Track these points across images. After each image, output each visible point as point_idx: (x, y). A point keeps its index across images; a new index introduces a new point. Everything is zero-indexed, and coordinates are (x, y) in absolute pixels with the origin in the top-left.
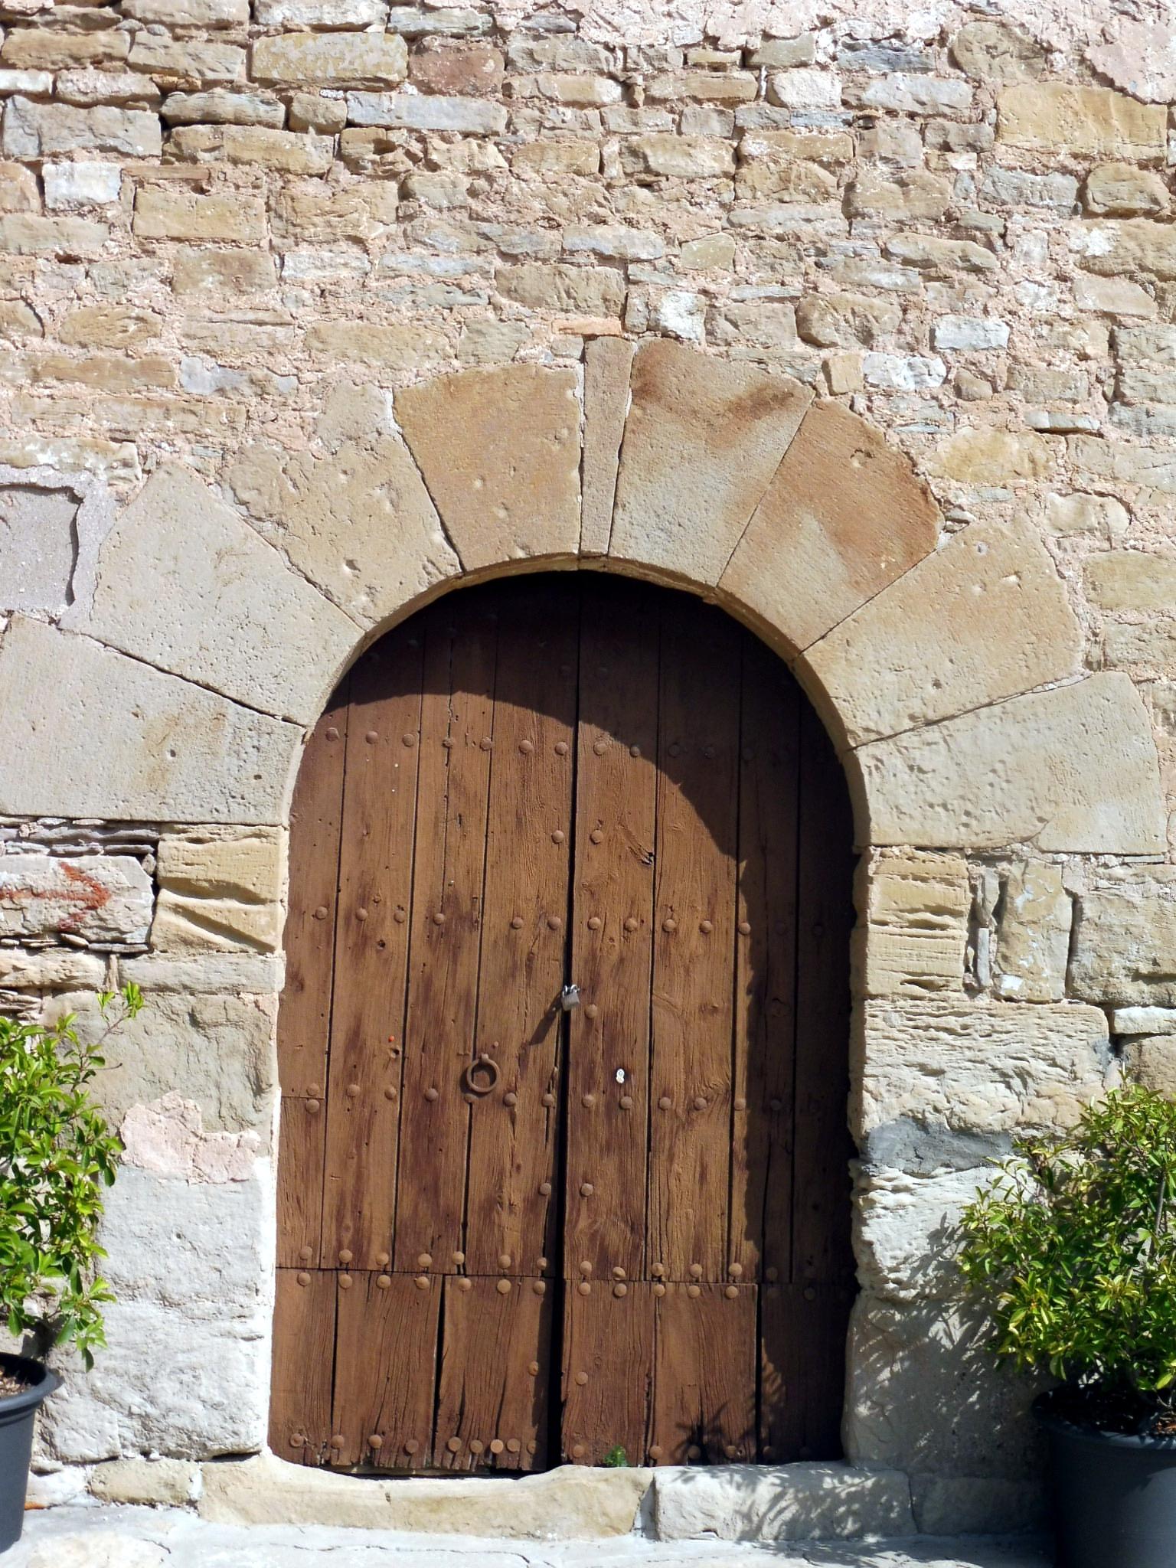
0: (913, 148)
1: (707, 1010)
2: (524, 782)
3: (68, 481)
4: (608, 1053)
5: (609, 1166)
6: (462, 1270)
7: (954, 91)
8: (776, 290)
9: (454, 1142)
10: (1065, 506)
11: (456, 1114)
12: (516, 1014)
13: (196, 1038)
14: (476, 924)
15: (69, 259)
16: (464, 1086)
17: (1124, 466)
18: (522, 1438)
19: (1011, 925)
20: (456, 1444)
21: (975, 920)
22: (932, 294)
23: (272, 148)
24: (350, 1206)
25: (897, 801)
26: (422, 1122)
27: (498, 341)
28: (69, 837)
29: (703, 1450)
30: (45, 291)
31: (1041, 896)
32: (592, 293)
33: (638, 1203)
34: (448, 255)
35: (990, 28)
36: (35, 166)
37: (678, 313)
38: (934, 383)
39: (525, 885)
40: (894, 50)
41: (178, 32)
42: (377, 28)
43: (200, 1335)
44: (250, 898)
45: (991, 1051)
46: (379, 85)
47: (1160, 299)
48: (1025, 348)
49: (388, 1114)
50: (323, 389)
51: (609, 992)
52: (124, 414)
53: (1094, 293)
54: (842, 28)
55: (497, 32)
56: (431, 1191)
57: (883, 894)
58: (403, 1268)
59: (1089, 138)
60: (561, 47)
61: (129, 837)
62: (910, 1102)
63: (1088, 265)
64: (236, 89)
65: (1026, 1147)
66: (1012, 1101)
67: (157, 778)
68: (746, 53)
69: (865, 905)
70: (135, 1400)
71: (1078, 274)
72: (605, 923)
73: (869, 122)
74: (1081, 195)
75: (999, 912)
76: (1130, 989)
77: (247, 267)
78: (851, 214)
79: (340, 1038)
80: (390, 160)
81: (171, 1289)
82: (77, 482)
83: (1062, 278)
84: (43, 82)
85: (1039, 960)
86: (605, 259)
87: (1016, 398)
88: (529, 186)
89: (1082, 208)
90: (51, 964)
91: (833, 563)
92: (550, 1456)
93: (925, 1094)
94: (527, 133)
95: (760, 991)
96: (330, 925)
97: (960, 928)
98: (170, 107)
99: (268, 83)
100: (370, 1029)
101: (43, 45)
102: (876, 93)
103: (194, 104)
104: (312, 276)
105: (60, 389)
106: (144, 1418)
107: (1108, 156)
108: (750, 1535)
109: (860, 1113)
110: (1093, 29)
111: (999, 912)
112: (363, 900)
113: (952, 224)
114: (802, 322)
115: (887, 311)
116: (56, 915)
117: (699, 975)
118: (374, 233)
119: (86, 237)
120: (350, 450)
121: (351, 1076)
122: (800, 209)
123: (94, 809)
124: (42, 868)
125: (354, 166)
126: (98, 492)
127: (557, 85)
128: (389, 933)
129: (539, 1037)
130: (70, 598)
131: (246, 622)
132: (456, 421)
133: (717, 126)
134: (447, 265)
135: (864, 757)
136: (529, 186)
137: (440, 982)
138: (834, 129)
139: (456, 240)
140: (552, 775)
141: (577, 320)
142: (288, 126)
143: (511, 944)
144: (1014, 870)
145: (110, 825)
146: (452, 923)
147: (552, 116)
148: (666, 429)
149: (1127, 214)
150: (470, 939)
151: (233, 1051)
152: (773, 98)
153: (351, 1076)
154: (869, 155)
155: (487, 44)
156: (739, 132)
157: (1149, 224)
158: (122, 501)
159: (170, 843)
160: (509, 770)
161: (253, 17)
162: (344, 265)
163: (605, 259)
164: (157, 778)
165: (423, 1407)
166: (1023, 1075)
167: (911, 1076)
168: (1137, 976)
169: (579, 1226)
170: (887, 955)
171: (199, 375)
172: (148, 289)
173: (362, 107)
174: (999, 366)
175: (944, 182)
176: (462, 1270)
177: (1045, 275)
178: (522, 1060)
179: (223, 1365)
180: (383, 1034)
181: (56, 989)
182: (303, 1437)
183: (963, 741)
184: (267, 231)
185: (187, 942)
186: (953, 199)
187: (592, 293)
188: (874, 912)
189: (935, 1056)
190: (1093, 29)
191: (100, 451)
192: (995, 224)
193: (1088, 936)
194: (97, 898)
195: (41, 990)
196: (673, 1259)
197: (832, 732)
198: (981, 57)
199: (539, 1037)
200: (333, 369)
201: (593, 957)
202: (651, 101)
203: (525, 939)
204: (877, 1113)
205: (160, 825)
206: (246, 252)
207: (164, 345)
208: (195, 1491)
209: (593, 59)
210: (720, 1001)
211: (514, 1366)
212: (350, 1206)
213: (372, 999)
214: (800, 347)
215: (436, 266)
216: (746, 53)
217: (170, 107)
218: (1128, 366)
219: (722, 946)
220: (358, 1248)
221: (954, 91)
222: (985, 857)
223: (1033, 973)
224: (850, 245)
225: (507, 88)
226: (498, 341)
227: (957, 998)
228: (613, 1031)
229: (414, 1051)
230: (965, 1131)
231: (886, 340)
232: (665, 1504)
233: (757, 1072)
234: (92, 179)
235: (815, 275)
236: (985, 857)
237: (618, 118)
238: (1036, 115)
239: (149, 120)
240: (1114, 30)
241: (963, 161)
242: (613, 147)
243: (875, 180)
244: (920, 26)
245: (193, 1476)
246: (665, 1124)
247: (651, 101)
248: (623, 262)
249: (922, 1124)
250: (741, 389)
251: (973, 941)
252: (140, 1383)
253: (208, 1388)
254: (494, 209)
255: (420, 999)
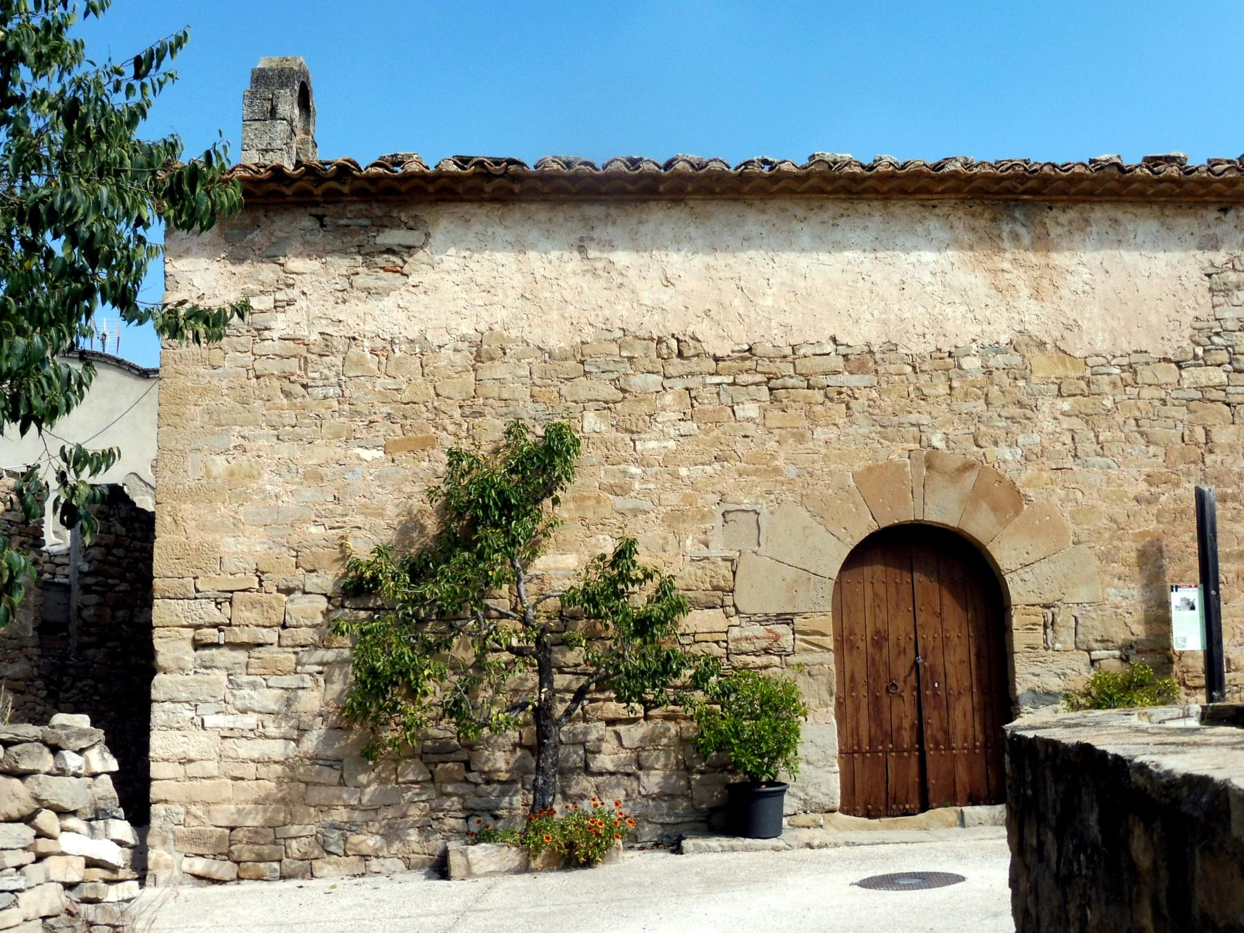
0: (1006, 381)
1: (962, 662)
2: (898, 593)
3: (755, 508)
4: (932, 678)
5: (936, 713)
6: (892, 750)
7: (1016, 360)
8: (967, 431)
9: (886, 710)
10: (1062, 493)
11: (886, 701)
12: (902, 668)
13: (811, 680)
14: (887, 639)
15: (745, 436)
16: (888, 691)
17: (1080, 479)
18: (914, 804)
19: (1057, 628)
20: (894, 807)
21: (1045, 627)
22: (1015, 428)
23: (806, 396)
24: (855, 732)
25: (1019, 591)
26: (876, 703)
27: (882, 454)
28: (767, 620)
29: (974, 801)
30: (740, 447)
31: (1064, 617)
32: (910, 436)
33: (945, 725)
34: (864, 428)
35: (1026, 338)
36: (732, 407)
37: (937, 441)
38: (1018, 457)
39: (899, 627)
40: (997, 349)
41: (771, 359)
42: (833, 354)
43: (820, 772)
44: (823, 635)
45: (1054, 667)
46: (836, 373)
47: (1087, 422)
48: (1046, 443)
49: (864, 702)
50: (830, 473)
51: (930, 657)
52: (769, 485)
53: (1066, 423)
54: (979, 342)
55: (871, 352)
56: (880, 725)
57: (1017, 620)
58: (873, 751)
59: (1060, 372)
60: (892, 356)
61: (785, 619)
62: (1030, 685)
63: (1063, 414)
64: (791, 377)
65: (1067, 697)
66: (1061, 682)
67: (792, 600)
68: (950, 353)
69: (1011, 624)
70: (801, 795)
71: (1060, 417)
72: (928, 637)
73: (991, 373)
74: (1059, 389)
75: (1052, 624)
76: (1095, 645)
77: (803, 436)
78: (987, 403)
79: (847, 678)
80: (845, 398)
81: (810, 759)
82: (757, 508)
83: (1055, 419)
84: (731, 379)
85: (1066, 638)
86: (913, 425)
87: (1044, 459)
88: (887, 402)
89: (1060, 394)
90: (764, 660)
91: (992, 517)
92: (924, 807)
93: (1034, 682)
94: (884, 385)
95: (978, 655)
96: (844, 643)
97: (1041, 629)
98: (772, 384)
99: (802, 375)
100: (857, 676)
101: (730, 368)
102: (992, 363)
103: (779, 382)
104: (822, 437)
105: (748, 479)
106: (805, 800)
107: (1066, 377)
108: (995, 824)
109: (1015, 689)
110: (1058, 335)
111: (1052, 624)
112: (851, 634)
113: (1020, 404)
114: (976, 441)
115: (1001, 434)
116: (765, 644)
117: (959, 650)
118: (840, 422)
119: (750, 429)
120: (841, 493)
121: (852, 690)
122: (973, 403)
123: (773, 610)
124: (759, 630)
125: (831, 400)
126: (764, 512)
127: (892, 369)
128: (862, 645)
129: (909, 675)
130: (759, 545)
131: (814, 548)
132: (874, 479)
133: (943, 378)
134: (864, 431)
135: (1007, 578)
136: (887, 402)
137: (877, 658)
138: (980, 376)
139: (866, 422)
140: (906, 590)
141: (906, 445)
142: (808, 388)
143: (898, 645)
144: (1056, 610)
145: (779, 615)
146: (880, 640)
147: (892, 378)
148: (938, 481)
149: (1075, 395)
150: (885, 644)
151: (822, 683)
152: (960, 367)
153: (852, 690)
154: (992, 384)
155: (868, 356)
156: (950, 380)
157: (1080, 398)
158: (772, 513)
159: (797, 620)
160: (892, 589)
161: (794, 353)
162: (832, 433)
163: (913, 425)
164: (792, 600)
165: (883, 795)
166: (1064, 674)
167: (1030, 677)
168: (1097, 641)
169: (928, 733)
170: (1020, 639)
171: (791, 471)
172: (772, 445)
173: (832, 380)
174: (1038, 450)
175: (1016, 390)
176: (892, 750)
177: (1051, 420)
178: (905, 682)
179: (828, 782)
180: (861, 677)
181: (766, 667)
182: (849, 807)
183: (1037, 571)
184: (807, 423)
185: (805, 650)
186: (1020, 396)
187: (910, 436)
188: (1014, 626)
189: (1037, 670)
190: (1058, 335)
191: (764, 498)
192: (1033, 403)
193: (1080, 629)
194: (777, 638)
195: (761, 668)
196: (957, 742)
197: (995, 570)
198: (1024, 347)
199: (909, 675)
200: (833, 467)
201: (924, 648)
202: (922, 371)
203: (902, 643)
204: (1020, 689)
205: (793, 614)
206: (801, 430)
207: (779, 463)
208: (822, 822)
209: (902, 359)
210: (965, 658)
211: (910, 781)
212: (855, 732)
213: (858, 666)
214: (976, 449)
215: (861, 431)
216: (950, 353)
217: (771, 384)
218: (1079, 446)
219: (965, 641)
220: (859, 745)
221: (1016, 360)
222: (1046, 606)
223: (1064, 642)
224: (988, 414)
225: (876, 371)
226: (882, 454)
227: (1042, 651)
228: (932, 671)
229: (871, 681)
230: (1048, 693)
231: (1002, 444)
232: (966, 816)
233: (979, 681)
234: (749, 410)
235: (979, 425)
236: (1046, 606)
237: (912, 378)
238: (1043, 367)
239: (765, 389)
240: (1065, 335)
241: (1021, 383)
242: (911, 388)
243: (994, 391)
244: (1004, 339)
245: (821, 818)
246: (952, 699)
247: (922, 371)
248: (918, 425)
249: (1034, 692)
250: (959, 464)
251: (1045, 633)
252: (803, 789)
253: (824, 789)
254: (877, 411)
255: (872, 664)
